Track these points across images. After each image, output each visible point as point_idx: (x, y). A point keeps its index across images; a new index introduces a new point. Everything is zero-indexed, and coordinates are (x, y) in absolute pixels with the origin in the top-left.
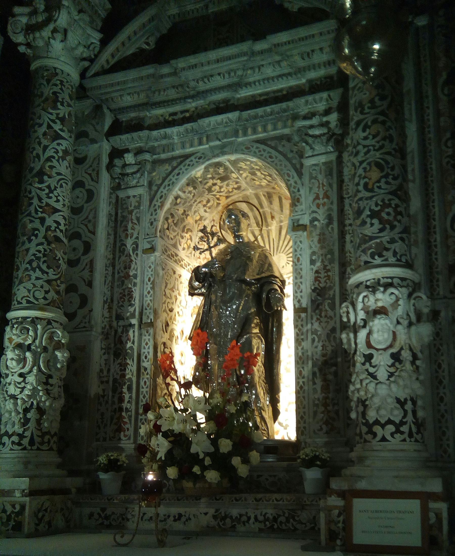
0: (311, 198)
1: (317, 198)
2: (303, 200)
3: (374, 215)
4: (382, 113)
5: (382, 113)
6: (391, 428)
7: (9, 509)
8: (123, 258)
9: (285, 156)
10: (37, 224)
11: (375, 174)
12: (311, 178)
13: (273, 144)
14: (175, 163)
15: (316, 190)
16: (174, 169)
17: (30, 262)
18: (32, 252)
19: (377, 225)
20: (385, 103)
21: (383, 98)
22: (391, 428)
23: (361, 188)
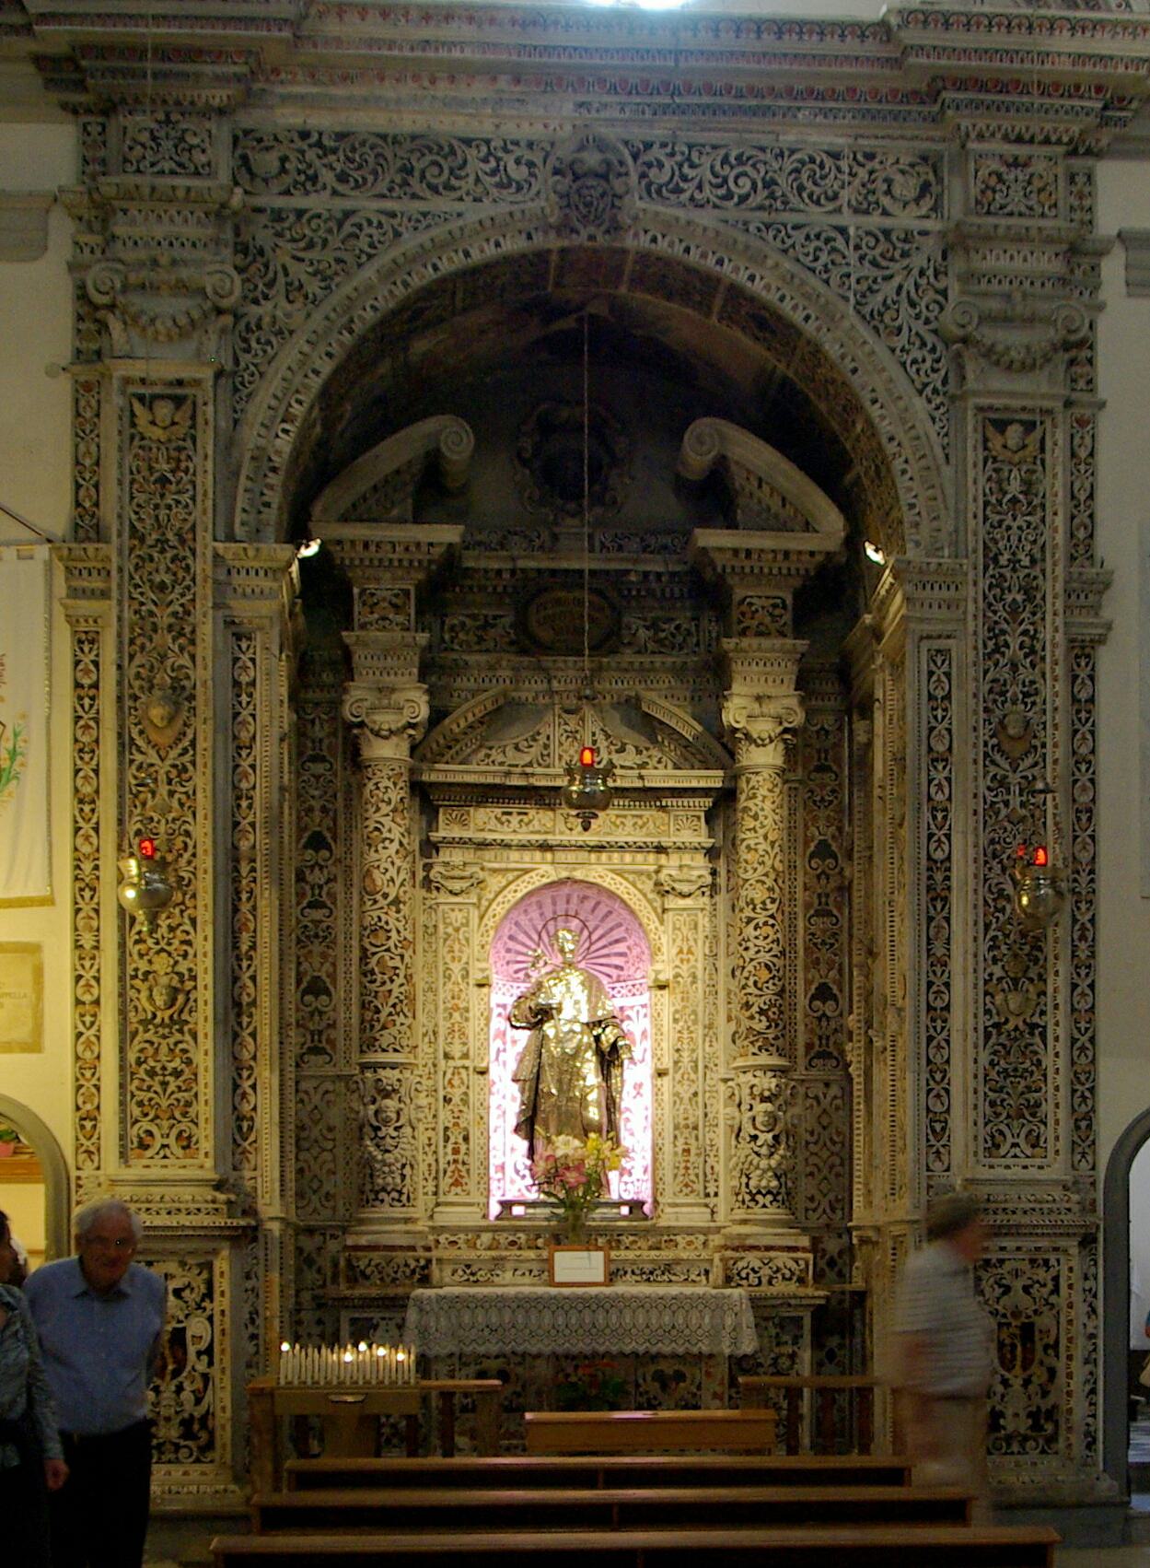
0: (675, 951)
1: (681, 951)
2: (664, 949)
3: (762, 1012)
4: (772, 916)
5: (772, 916)
6: (770, 1198)
7: (413, 1264)
8: (450, 986)
9: (645, 895)
10: (397, 962)
11: (765, 975)
12: (675, 928)
13: (631, 877)
14: (511, 876)
15: (679, 942)
16: (510, 883)
17: (394, 1006)
18: (395, 994)
19: (765, 1023)
20: (775, 906)
21: (773, 901)
22: (770, 1198)
23: (751, 983)
